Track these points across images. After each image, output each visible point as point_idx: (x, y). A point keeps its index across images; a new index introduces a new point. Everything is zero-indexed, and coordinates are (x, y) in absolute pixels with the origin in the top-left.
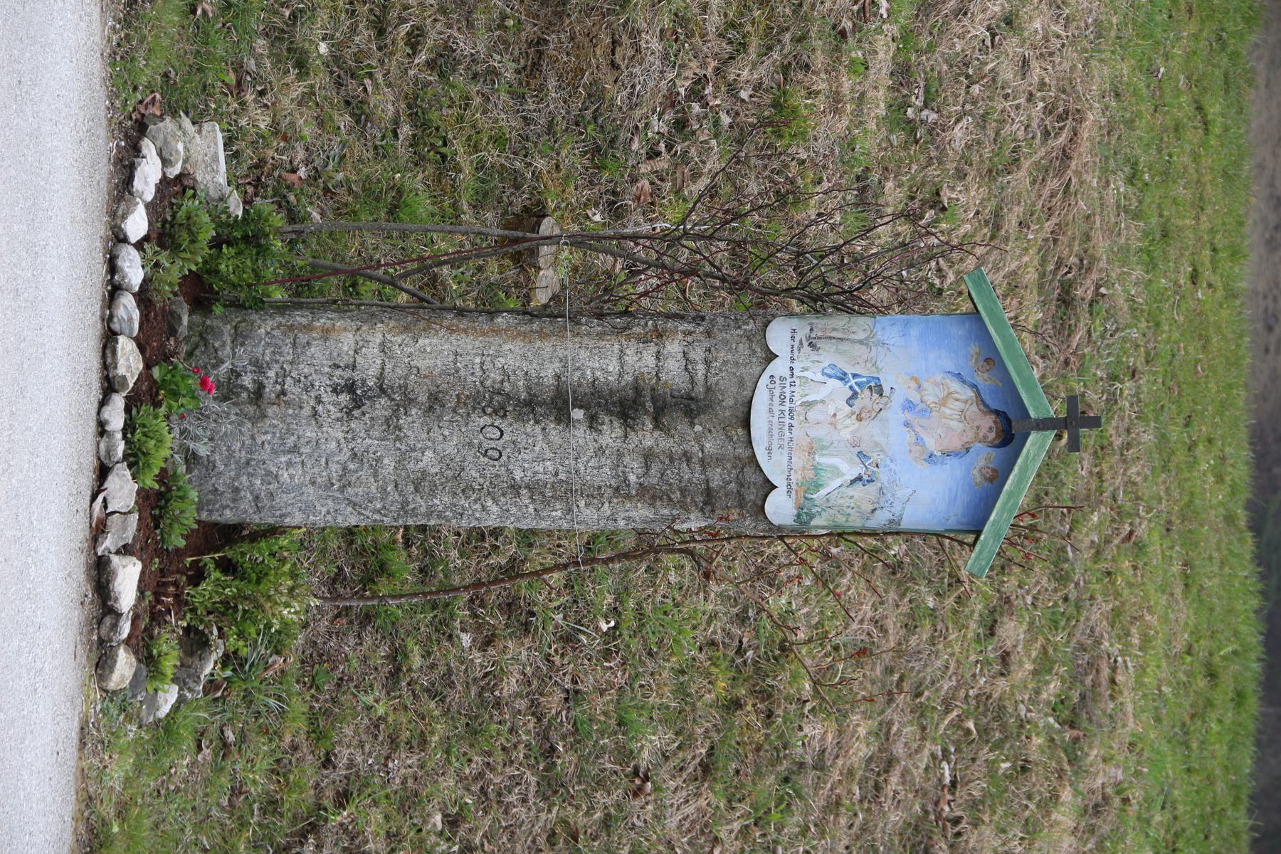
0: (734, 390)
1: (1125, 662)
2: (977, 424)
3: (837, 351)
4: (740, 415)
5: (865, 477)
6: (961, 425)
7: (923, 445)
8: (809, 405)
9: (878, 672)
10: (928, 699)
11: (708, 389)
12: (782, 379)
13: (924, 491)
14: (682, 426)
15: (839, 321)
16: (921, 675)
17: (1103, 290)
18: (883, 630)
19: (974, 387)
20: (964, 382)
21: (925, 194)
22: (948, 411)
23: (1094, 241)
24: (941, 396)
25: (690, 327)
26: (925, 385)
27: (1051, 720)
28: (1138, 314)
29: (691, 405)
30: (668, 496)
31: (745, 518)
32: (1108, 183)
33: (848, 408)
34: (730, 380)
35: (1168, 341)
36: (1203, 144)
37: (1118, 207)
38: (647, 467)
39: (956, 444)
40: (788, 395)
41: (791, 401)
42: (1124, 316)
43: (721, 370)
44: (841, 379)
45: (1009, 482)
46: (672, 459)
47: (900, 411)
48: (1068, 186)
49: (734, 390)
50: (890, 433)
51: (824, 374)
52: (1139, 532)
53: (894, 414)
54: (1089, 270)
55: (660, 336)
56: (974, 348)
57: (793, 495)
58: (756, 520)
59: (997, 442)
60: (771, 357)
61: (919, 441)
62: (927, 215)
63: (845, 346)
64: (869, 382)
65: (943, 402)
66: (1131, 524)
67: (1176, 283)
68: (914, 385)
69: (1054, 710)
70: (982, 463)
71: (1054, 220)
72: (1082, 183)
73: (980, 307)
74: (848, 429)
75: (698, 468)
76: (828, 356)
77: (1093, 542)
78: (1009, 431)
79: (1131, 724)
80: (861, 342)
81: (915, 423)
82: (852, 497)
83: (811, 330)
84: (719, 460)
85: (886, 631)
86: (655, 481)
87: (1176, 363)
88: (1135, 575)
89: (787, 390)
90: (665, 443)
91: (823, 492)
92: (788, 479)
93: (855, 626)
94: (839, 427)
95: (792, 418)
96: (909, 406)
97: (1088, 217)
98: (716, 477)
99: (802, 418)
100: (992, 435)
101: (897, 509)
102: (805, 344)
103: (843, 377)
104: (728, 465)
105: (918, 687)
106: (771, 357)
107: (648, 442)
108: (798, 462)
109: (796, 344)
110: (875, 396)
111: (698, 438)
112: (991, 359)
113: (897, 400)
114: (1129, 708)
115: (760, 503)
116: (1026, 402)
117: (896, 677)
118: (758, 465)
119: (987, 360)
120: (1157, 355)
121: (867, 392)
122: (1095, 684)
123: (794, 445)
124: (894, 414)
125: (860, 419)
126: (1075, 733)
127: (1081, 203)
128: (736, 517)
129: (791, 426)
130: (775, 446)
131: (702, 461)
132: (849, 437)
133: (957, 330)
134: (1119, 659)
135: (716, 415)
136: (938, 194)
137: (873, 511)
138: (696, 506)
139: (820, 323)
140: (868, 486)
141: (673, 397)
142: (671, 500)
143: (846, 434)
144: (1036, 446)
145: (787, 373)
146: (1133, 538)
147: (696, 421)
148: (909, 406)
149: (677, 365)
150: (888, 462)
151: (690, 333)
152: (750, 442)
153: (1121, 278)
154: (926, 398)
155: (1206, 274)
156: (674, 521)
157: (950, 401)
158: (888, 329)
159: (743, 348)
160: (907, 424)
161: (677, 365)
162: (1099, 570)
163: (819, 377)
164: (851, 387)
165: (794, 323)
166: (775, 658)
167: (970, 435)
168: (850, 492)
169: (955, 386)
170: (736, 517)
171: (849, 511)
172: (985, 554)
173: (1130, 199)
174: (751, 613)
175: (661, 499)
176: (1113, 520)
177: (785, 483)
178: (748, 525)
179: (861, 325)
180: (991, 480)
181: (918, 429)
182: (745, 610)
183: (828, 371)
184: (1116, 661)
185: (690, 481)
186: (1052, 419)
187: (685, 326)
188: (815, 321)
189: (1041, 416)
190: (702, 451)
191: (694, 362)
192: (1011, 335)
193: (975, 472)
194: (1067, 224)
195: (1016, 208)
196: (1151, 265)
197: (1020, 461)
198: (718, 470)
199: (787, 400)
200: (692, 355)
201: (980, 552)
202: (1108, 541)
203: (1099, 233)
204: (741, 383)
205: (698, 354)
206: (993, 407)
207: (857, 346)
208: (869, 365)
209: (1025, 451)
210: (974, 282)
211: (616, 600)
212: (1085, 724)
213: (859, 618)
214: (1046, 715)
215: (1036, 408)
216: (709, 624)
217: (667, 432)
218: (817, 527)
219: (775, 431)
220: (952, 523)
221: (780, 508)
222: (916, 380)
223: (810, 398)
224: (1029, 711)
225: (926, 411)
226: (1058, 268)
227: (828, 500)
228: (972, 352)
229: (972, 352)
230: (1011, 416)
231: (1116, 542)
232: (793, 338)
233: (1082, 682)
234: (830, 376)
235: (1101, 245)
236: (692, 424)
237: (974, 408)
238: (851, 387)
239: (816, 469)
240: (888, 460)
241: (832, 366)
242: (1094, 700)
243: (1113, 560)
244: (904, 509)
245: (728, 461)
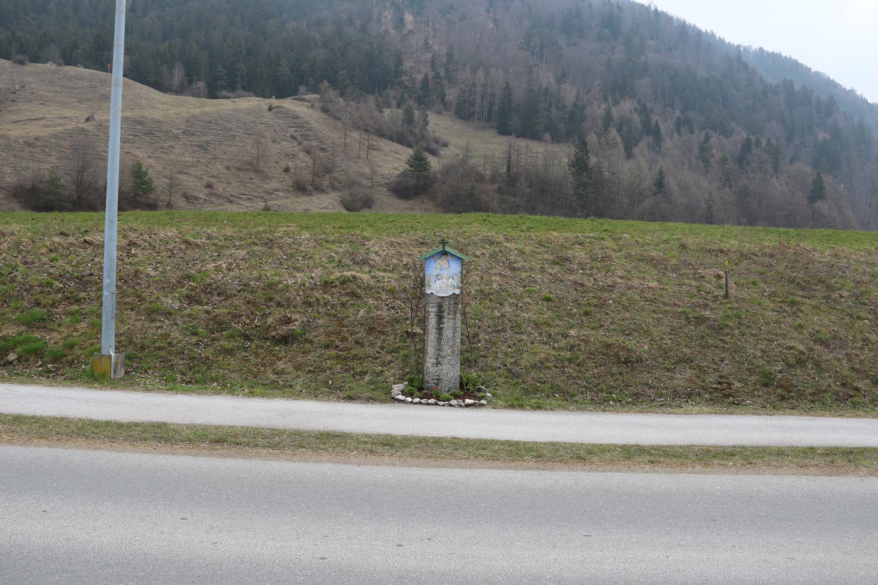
13: (455, 268)
29: (440, 307)
50: (445, 273)
53: (442, 272)
76: (432, 283)
78: (445, 253)
98: (452, 302)
112: (433, 256)
124: (442, 272)
133: (428, 262)
144: (447, 249)
158: (427, 273)
221: (458, 292)
235: (413, 238)
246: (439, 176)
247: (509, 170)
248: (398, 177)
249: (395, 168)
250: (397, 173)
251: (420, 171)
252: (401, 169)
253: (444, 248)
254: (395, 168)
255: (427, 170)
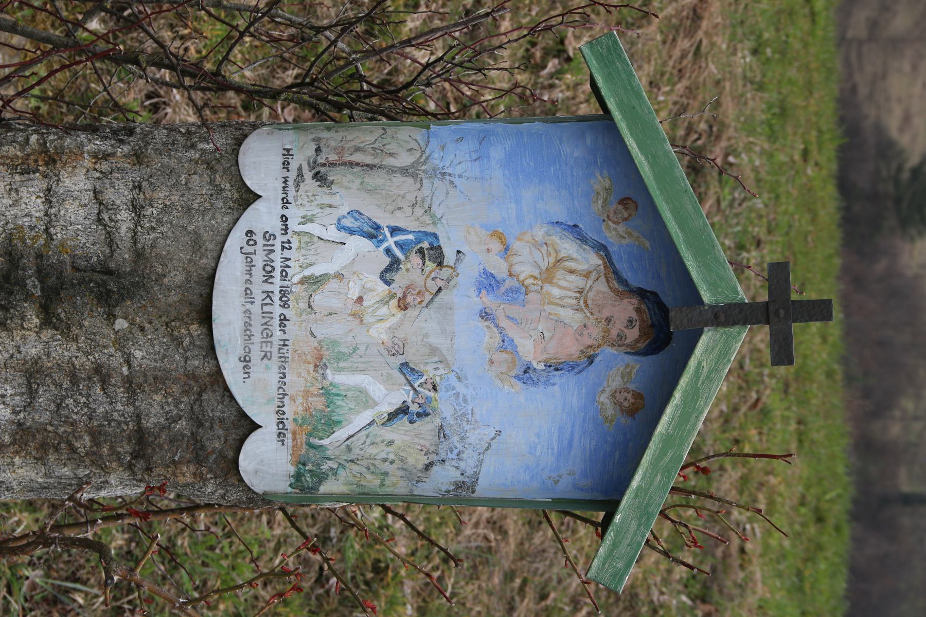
0: (184, 256)
1: (753, 529)
2: (606, 313)
3: (364, 188)
4: (197, 300)
5: (414, 408)
6: (579, 316)
7: (514, 351)
8: (315, 282)
9: (496, 580)
10: (555, 600)
11: (139, 255)
12: (268, 236)
13: (515, 430)
14: (93, 321)
15: (364, 136)
16: (546, 576)
17: (731, 159)
18: (503, 532)
19: (601, 248)
20: (583, 240)
21: (546, 41)
22: (556, 292)
23: (724, 107)
24: (544, 265)
25: (105, 146)
26: (516, 246)
27: (684, 598)
28: (762, 184)
29: (108, 283)
30: (70, 444)
31: (205, 481)
32: (735, 50)
33: (382, 288)
34: (176, 239)
35: (786, 212)
36: (811, 33)
37: (745, 77)
38: (32, 394)
39: (572, 349)
40: (278, 265)
41: (284, 276)
42: (750, 184)
43: (160, 222)
44: (371, 237)
45: (665, 419)
46: (74, 379)
47: (473, 293)
48: (698, 48)
49: (184, 256)
50: (456, 331)
51: (340, 227)
52: (764, 399)
53: (464, 298)
54: (718, 137)
55: (51, 161)
56: (601, 181)
57: (289, 440)
58: (225, 484)
59: (641, 346)
60: (248, 198)
61: (506, 345)
62: (550, 65)
63: (376, 179)
64: (418, 241)
65: (547, 276)
66: (758, 392)
67: (792, 158)
68: (496, 246)
69: (686, 586)
70: (616, 383)
71: (685, 83)
72: (713, 44)
73: (611, 105)
74: (383, 324)
75: (121, 394)
76: (348, 196)
77: (722, 412)
78: (664, 324)
79: (760, 588)
80: (404, 171)
81: (499, 314)
82: (391, 443)
83: (318, 150)
84: (160, 380)
85: (506, 533)
86: (45, 417)
87: (793, 234)
88: (761, 440)
89: (277, 257)
90: (63, 351)
91: (341, 434)
92: (280, 412)
93: (468, 532)
94: (368, 319)
95: (285, 305)
96: (488, 282)
97: (718, 83)
98: (154, 409)
99: (303, 305)
100: (633, 334)
101: (469, 463)
102: (308, 175)
103: (373, 233)
104: (176, 389)
105: (543, 589)
106: (248, 198)
107: (32, 350)
108: (297, 381)
109: (292, 175)
110: (430, 265)
111: (121, 342)
112: (633, 200)
113: (469, 271)
114: (758, 575)
115: (231, 454)
116: (694, 274)
117: (518, 581)
118: (227, 389)
119: (624, 202)
120: (777, 225)
121: (416, 260)
122: (726, 555)
123: (289, 352)
124: (464, 298)
125: (403, 306)
126: (707, 608)
127: (712, 67)
128: (189, 479)
129: (284, 319)
130: (256, 355)
131: (129, 383)
132: (384, 337)
133: (571, 148)
134: (748, 527)
135: (153, 302)
136: (562, 42)
137: (428, 466)
138: (119, 460)
139: (332, 137)
140: (419, 423)
141: (76, 269)
142: (74, 450)
143: (379, 333)
144: (715, 356)
145: (275, 226)
146: (760, 406)
147: (118, 311)
148: (488, 282)
149: (82, 213)
150: (453, 381)
151: (106, 156)
152: (211, 349)
153: (749, 148)
154: (517, 269)
155: (814, 154)
156: (80, 489)
157: (560, 274)
158: (450, 148)
159: (199, 182)
160: (485, 315)
161: (82, 213)
162: (728, 439)
163: (333, 233)
164: (388, 251)
165: (289, 139)
166: (367, 583)
167: (596, 332)
168: (388, 433)
169: (569, 247)
170: (189, 479)
171: (387, 467)
172: (623, 549)
173: (754, 71)
174: (334, 532)
175: (57, 449)
176: (740, 388)
177: (274, 418)
178: (211, 490)
179: (403, 141)
180: (631, 412)
181: (504, 323)
182: (326, 529)
183: (348, 222)
184: (744, 529)
185: (107, 417)
186: (741, 305)
187: (98, 144)
188: (325, 135)
189: (723, 300)
190: (128, 362)
191: (113, 208)
192: (667, 153)
193: (604, 398)
194: (697, 88)
195: (646, 66)
196: (772, 137)
197: (684, 381)
198: (158, 398)
199: (277, 273)
200: (109, 195)
201: (615, 545)
202: (736, 410)
203: (729, 99)
204: (197, 244)
205: (119, 194)
206: (635, 283)
207: (398, 179)
208: (419, 211)
209: (692, 363)
210: (600, 58)
211: (130, 541)
212: (716, 596)
213: (474, 520)
214: (679, 592)
215: (713, 287)
216: (276, 550)
217: (66, 330)
218: (330, 497)
219: (257, 329)
220: (565, 488)
221: (265, 462)
222: (500, 237)
223: (317, 270)
224: (662, 593)
225: (518, 292)
226: (688, 135)
227: (349, 449)
228: (597, 187)
229: (597, 187)
230: (667, 300)
231: (744, 409)
232: (286, 165)
233: (714, 556)
234: (351, 232)
235: (730, 109)
236: (111, 318)
237: (602, 286)
238: (388, 251)
239: (328, 394)
240: (452, 376)
241: (355, 214)
242: (725, 572)
243: (741, 428)
244: (481, 462)
245: (175, 381)
246: (881, 265)
247: (908, 500)
248: (879, 129)
249: (907, 119)
250: (893, 124)
251: (898, 201)
252: (904, 140)
253: (730, 315)
254: (907, 119)
255: (904, 223)
